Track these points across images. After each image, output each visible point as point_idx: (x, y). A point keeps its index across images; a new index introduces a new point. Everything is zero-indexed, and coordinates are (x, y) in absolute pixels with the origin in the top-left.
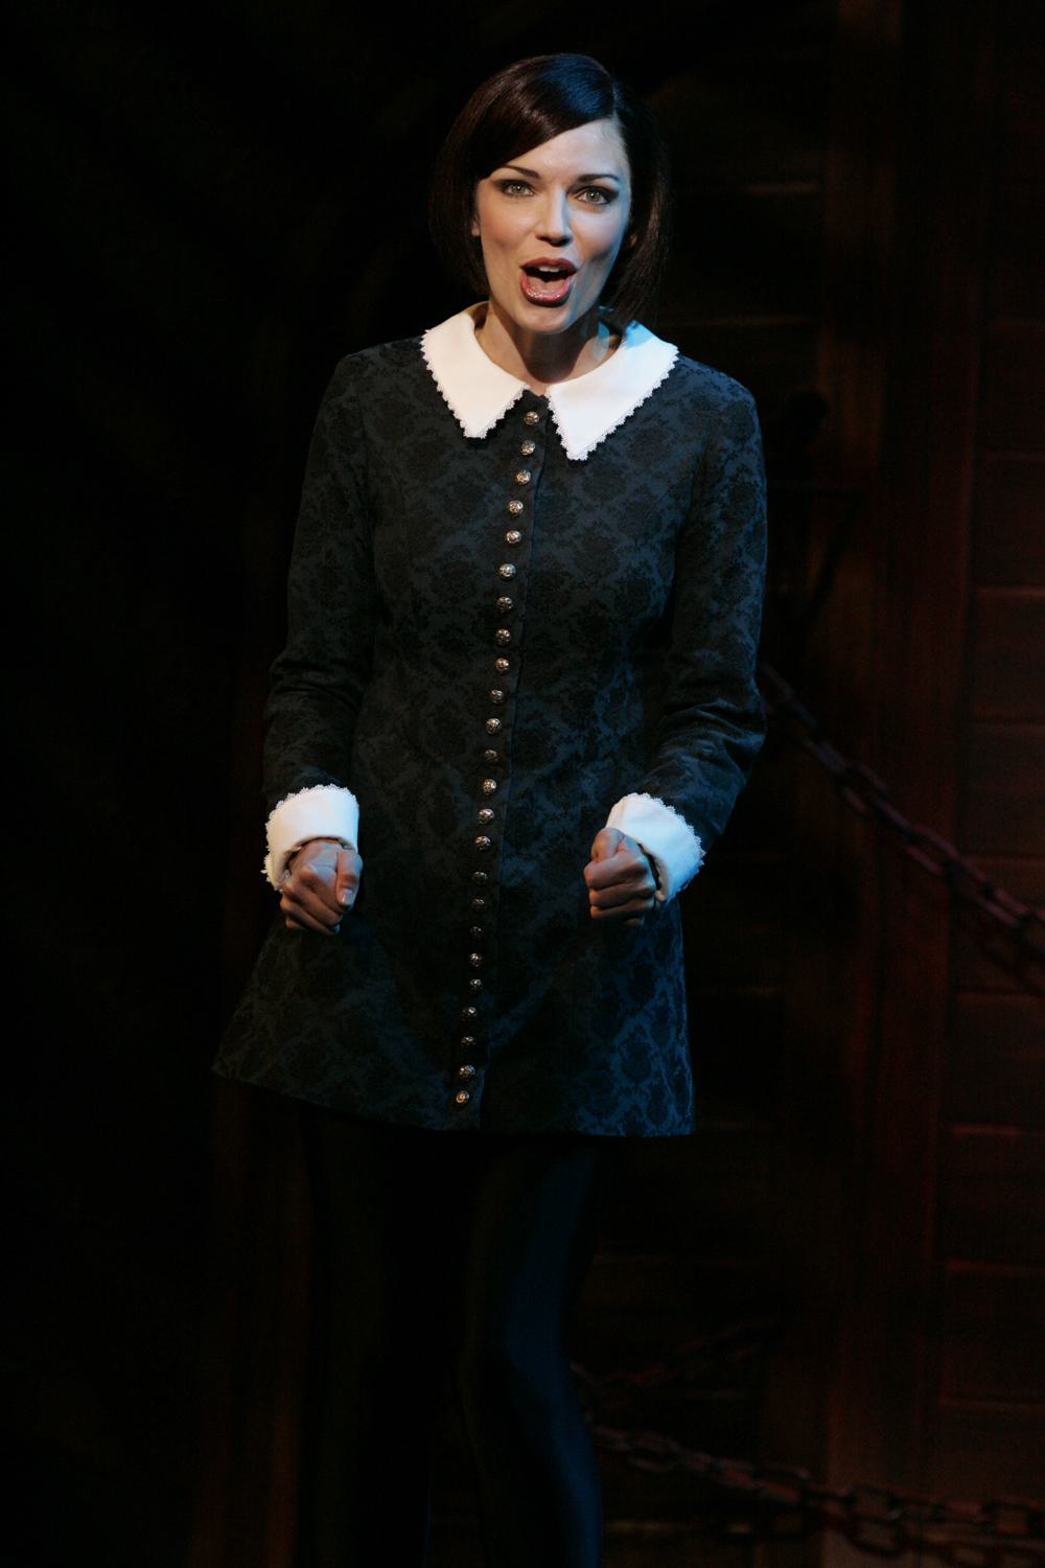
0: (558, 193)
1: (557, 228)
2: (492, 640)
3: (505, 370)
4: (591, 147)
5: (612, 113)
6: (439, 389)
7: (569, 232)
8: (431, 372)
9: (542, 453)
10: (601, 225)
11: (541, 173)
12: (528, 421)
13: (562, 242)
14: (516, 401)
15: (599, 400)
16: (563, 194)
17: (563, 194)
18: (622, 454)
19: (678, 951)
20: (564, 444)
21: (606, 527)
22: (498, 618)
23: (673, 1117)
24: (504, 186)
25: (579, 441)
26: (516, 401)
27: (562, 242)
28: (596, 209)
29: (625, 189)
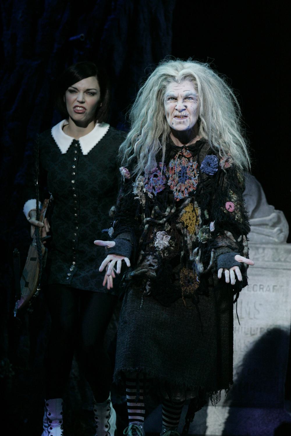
7: (84, 100)
9: (78, 153)
10: (90, 101)
12: (75, 146)
16: (214, 392)
19: (143, 233)
20: (82, 151)
22: (73, 192)
23: (222, 121)
24: (72, 92)
25: (85, 151)
28: (213, 73)
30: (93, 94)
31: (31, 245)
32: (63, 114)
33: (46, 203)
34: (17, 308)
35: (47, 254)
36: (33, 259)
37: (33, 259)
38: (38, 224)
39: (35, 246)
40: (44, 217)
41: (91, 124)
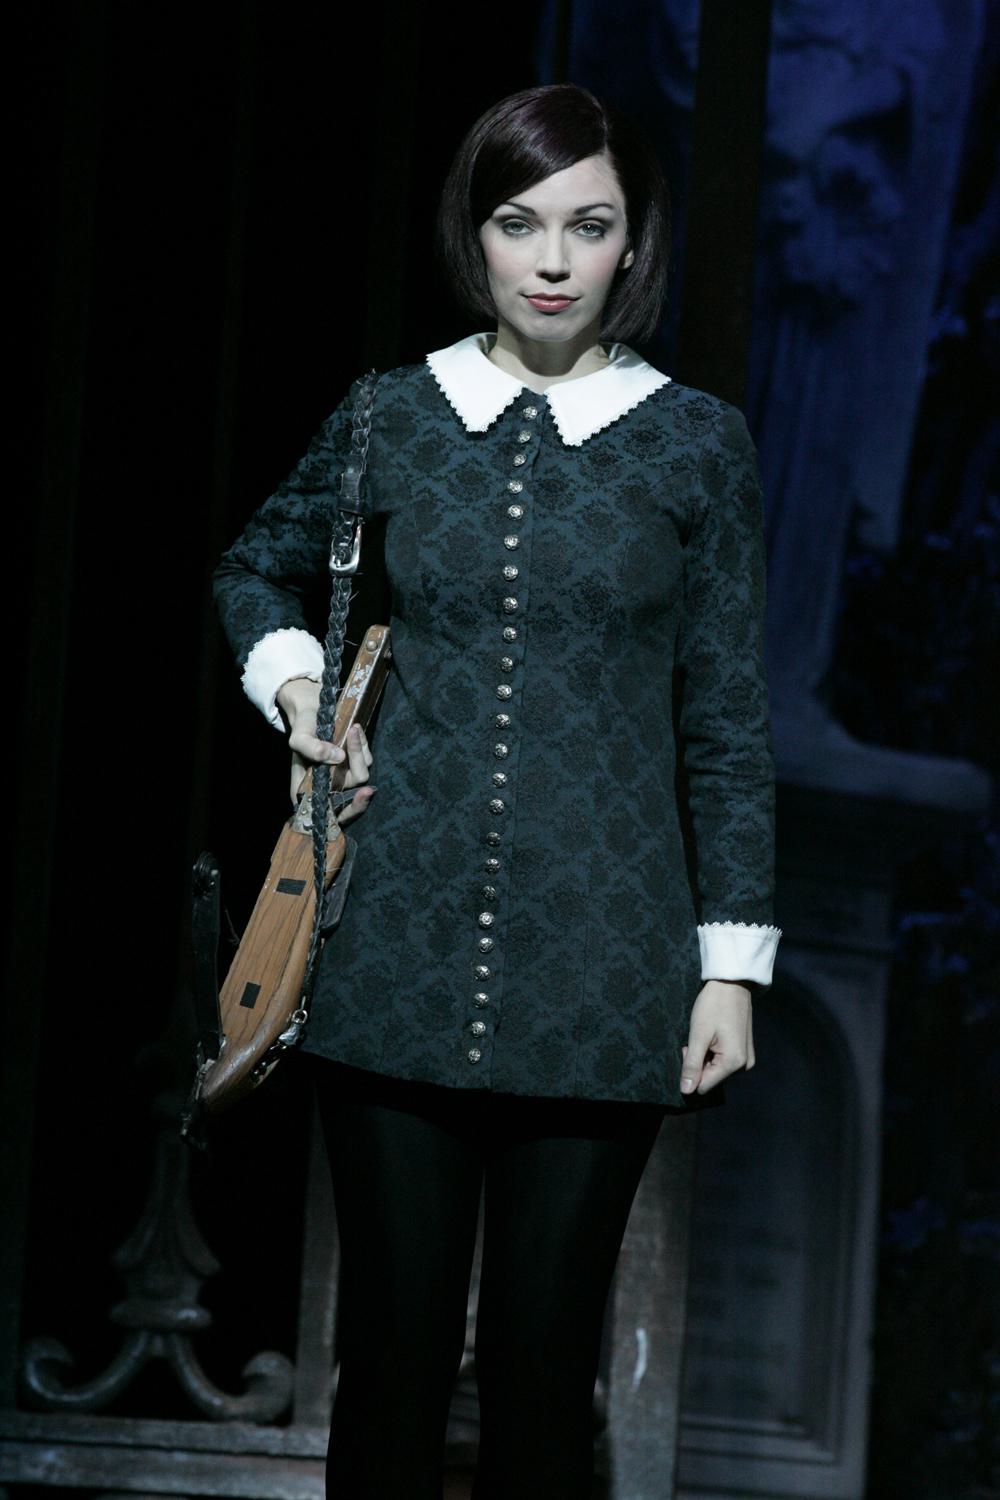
0: (554, 230)
1: (553, 265)
2: (501, 612)
3: (526, 190)
4: (583, 183)
5: (603, 145)
6: (442, 390)
7: (566, 268)
8: (434, 376)
10: (590, 262)
11: (536, 210)
12: (526, 417)
13: (562, 277)
14: (515, 399)
15: (597, 397)
16: (558, 233)
17: (558, 233)
18: (611, 577)
21: (605, 504)
22: (507, 587)
24: (509, 225)
26: (515, 399)
27: (562, 277)
29: (618, 214)
30: (602, 228)
31: (287, 825)
32: (470, 313)
33: (371, 644)
34: (200, 1093)
35: (350, 865)
36: (290, 886)
37: (290, 886)
38: (322, 753)
39: (306, 828)
40: (351, 721)
41: (588, 357)
